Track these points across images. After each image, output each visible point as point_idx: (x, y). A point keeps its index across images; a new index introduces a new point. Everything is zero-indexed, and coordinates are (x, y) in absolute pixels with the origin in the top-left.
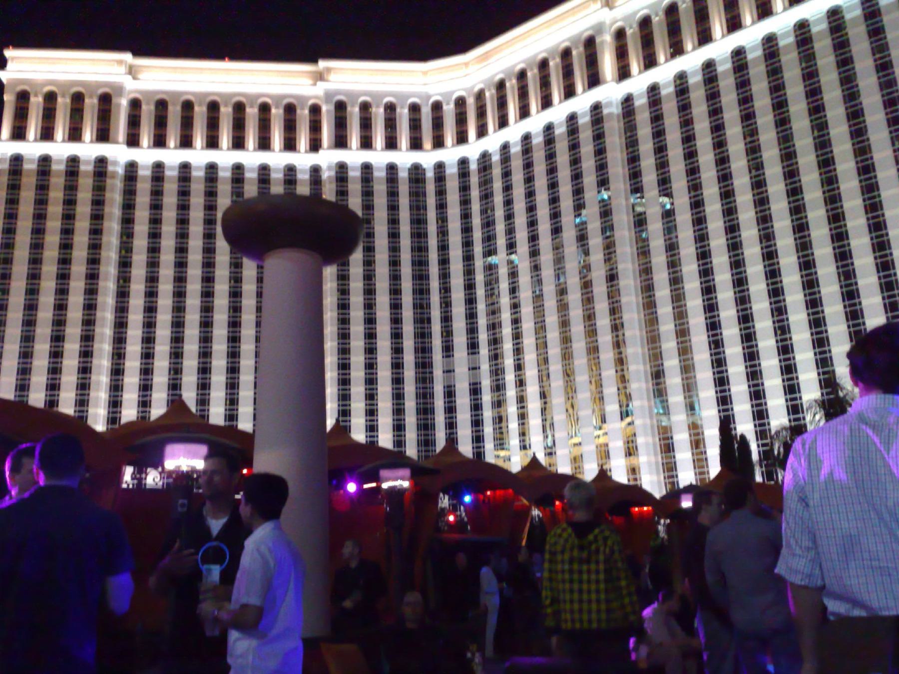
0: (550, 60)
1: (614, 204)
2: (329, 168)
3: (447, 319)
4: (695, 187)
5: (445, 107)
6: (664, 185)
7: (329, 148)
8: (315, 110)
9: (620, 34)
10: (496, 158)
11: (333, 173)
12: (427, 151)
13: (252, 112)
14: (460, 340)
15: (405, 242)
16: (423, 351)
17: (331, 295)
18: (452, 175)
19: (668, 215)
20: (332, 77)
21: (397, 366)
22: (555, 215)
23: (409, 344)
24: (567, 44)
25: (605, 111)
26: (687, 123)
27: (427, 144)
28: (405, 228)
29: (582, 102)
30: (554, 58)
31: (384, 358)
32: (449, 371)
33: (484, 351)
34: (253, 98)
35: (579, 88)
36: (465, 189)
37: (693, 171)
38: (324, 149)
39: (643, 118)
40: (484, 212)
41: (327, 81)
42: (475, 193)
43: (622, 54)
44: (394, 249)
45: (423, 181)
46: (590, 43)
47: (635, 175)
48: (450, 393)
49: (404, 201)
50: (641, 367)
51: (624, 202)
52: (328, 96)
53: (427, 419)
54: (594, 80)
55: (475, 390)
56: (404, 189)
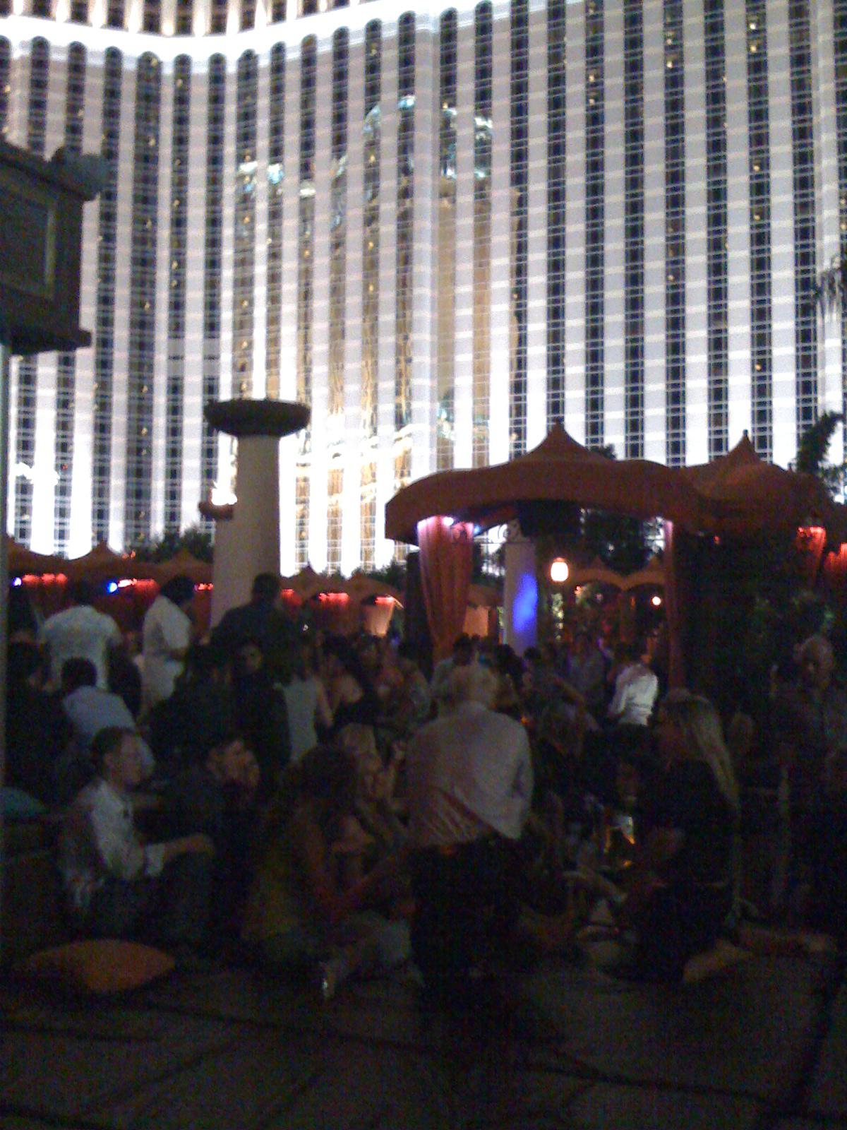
1: (418, 113)
2: (23, 45)
4: (519, 110)
6: (483, 98)
10: (264, 62)
14: (194, 316)
19: (481, 189)
22: (340, 118)
23: (119, 419)
25: (419, 27)
32: (176, 358)
33: (226, 335)
37: (519, 88)
40: (241, 97)
42: (231, 109)
45: (158, 78)
47: (448, 80)
48: (175, 388)
56: (128, 88)
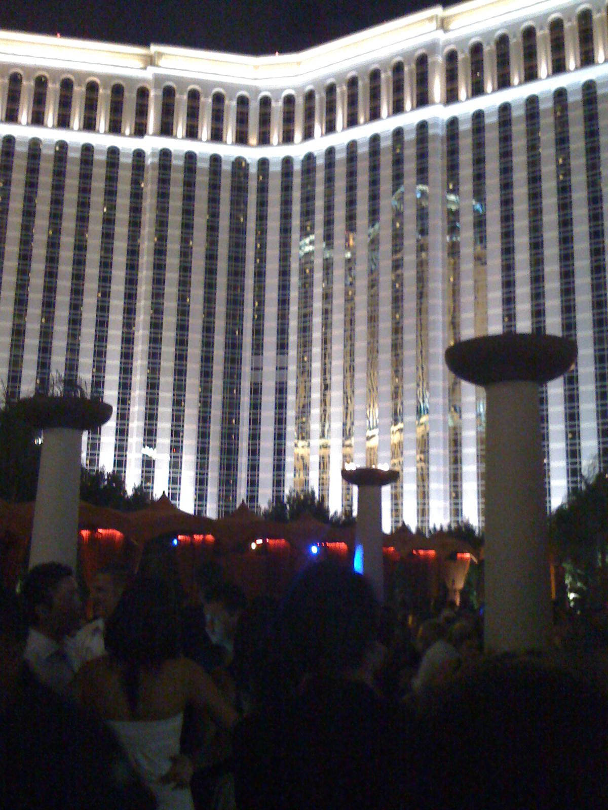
0: (382, 72)
2: (153, 154)
3: (254, 468)
5: (273, 104)
7: (154, 134)
8: (143, 93)
9: (452, 57)
10: (320, 162)
11: (156, 160)
12: (252, 146)
13: (79, 91)
14: (270, 339)
15: (222, 280)
16: (233, 345)
17: (146, 283)
18: (275, 173)
20: (162, 62)
21: (207, 359)
23: (220, 324)
24: (399, 59)
25: (431, 131)
26: (506, 154)
27: (253, 140)
28: (222, 265)
29: (410, 118)
30: (386, 71)
31: (194, 351)
32: (257, 369)
33: (293, 352)
34: (81, 75)
35: (408, 105)
36: (287, 188)
38: (148, 135)
39: (466, 143)
41: (158, 66)
43: (451, 77)
44: (208, 344)
45: (246, 176)
46: (422, 61)
48: (256, 390)
49: (225, 195)
50: (441, 451)
51: (440, 207)
52: (158, 79)
53: (235, 266)
54: (423, 100)
55: (281, 390)
56: (226, 183)
